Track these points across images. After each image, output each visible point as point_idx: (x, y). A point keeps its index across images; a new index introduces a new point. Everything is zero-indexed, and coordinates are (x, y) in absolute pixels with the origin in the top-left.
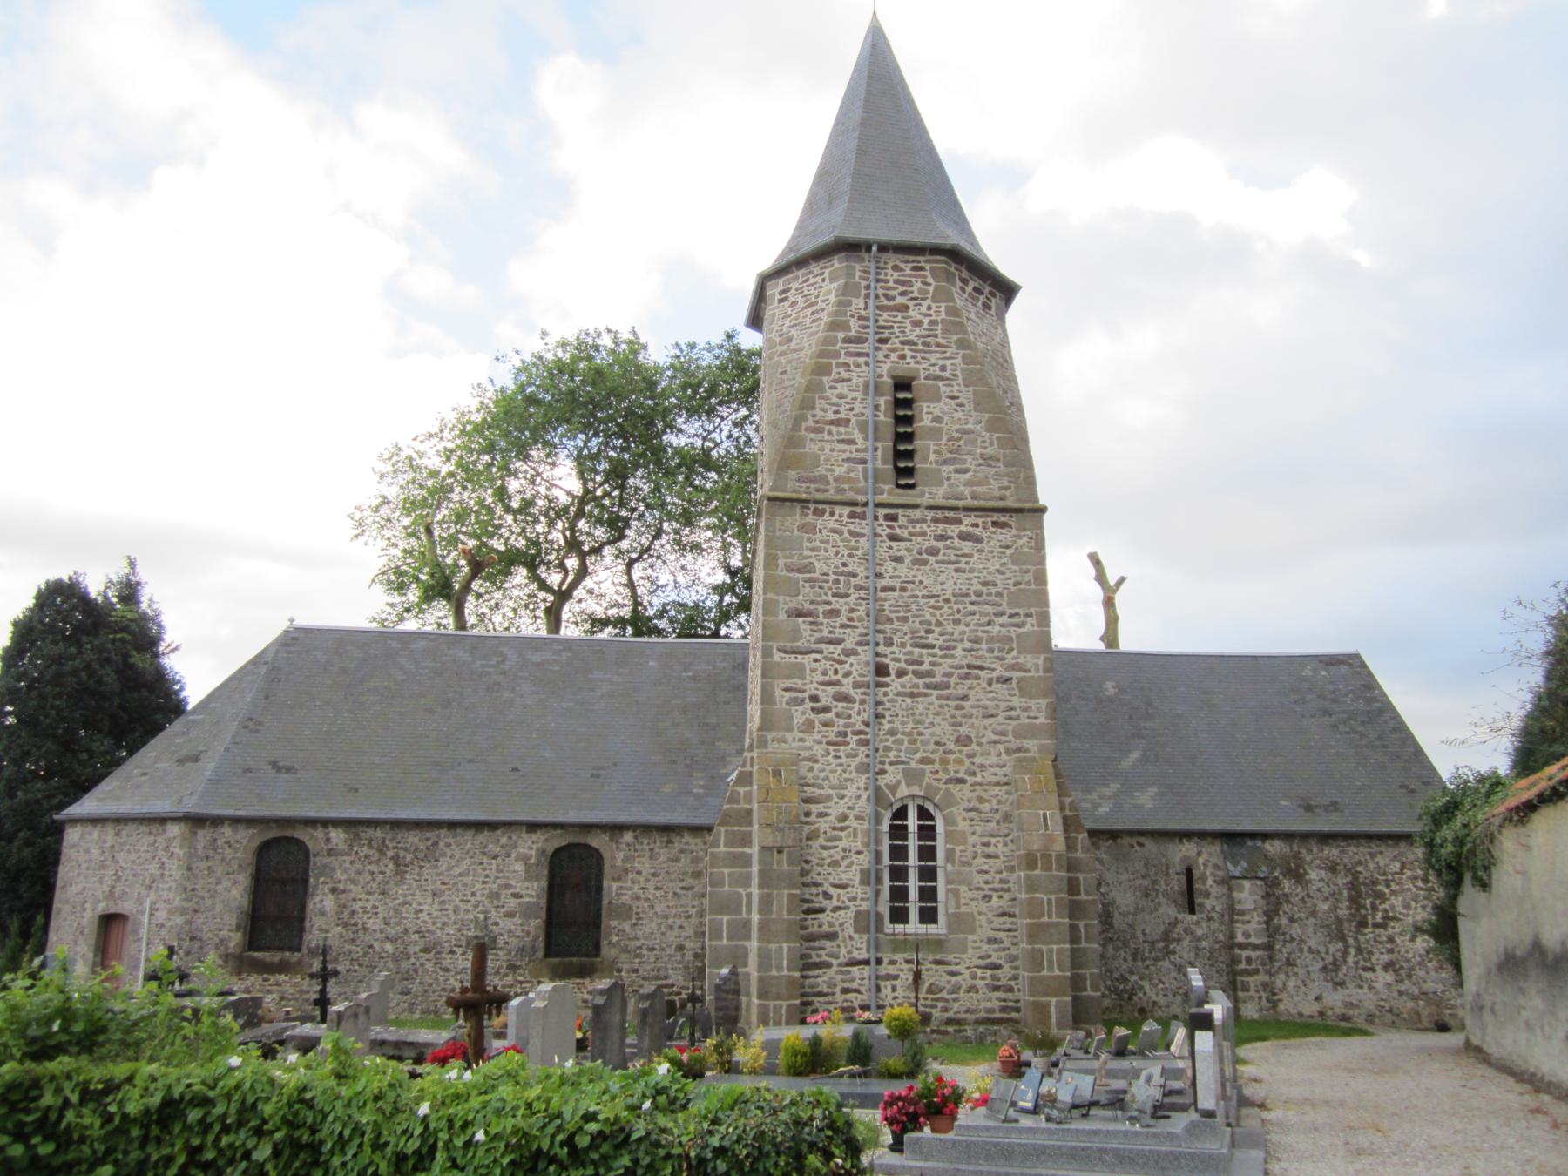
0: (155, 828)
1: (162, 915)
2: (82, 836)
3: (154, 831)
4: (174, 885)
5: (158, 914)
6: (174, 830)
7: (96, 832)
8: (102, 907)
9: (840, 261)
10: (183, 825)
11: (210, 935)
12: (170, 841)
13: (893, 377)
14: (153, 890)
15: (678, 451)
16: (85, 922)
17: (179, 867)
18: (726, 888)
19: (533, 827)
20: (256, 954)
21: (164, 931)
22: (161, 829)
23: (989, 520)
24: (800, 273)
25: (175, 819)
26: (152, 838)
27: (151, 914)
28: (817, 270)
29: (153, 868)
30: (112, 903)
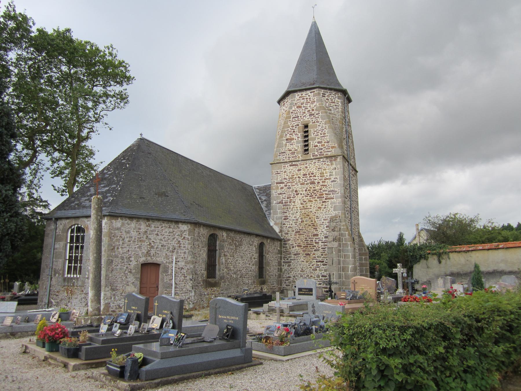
0: (173, 225)
1: (181, 264)
2: (123, 224)
3: (172, 227)
4: (187, 251)
5: (179, 263)
6: (184, 227)
7: (133, 224)
8: (142, 260)
9: (340, 94)
10: (189, 226)
11: (199, 273)
12: (182, 232)
13: (303, 124)
14: (175, 253)
15: (42, 98)
16: (132, 267)
17: (189, 244)
18: (363, 257)
19: (257, 235)
20: (210, 280)
21: (183, 271)
22: (176, 226)
23: (288, 165)
24: (329, 91)
25: (184, 222)
26: (171, 230)
27: (176, 264)
28: (334, 93)
29: (174, 243)
30: (149, 258)
